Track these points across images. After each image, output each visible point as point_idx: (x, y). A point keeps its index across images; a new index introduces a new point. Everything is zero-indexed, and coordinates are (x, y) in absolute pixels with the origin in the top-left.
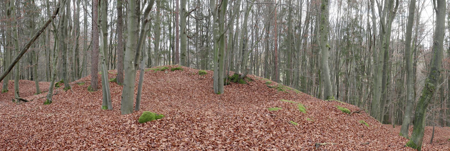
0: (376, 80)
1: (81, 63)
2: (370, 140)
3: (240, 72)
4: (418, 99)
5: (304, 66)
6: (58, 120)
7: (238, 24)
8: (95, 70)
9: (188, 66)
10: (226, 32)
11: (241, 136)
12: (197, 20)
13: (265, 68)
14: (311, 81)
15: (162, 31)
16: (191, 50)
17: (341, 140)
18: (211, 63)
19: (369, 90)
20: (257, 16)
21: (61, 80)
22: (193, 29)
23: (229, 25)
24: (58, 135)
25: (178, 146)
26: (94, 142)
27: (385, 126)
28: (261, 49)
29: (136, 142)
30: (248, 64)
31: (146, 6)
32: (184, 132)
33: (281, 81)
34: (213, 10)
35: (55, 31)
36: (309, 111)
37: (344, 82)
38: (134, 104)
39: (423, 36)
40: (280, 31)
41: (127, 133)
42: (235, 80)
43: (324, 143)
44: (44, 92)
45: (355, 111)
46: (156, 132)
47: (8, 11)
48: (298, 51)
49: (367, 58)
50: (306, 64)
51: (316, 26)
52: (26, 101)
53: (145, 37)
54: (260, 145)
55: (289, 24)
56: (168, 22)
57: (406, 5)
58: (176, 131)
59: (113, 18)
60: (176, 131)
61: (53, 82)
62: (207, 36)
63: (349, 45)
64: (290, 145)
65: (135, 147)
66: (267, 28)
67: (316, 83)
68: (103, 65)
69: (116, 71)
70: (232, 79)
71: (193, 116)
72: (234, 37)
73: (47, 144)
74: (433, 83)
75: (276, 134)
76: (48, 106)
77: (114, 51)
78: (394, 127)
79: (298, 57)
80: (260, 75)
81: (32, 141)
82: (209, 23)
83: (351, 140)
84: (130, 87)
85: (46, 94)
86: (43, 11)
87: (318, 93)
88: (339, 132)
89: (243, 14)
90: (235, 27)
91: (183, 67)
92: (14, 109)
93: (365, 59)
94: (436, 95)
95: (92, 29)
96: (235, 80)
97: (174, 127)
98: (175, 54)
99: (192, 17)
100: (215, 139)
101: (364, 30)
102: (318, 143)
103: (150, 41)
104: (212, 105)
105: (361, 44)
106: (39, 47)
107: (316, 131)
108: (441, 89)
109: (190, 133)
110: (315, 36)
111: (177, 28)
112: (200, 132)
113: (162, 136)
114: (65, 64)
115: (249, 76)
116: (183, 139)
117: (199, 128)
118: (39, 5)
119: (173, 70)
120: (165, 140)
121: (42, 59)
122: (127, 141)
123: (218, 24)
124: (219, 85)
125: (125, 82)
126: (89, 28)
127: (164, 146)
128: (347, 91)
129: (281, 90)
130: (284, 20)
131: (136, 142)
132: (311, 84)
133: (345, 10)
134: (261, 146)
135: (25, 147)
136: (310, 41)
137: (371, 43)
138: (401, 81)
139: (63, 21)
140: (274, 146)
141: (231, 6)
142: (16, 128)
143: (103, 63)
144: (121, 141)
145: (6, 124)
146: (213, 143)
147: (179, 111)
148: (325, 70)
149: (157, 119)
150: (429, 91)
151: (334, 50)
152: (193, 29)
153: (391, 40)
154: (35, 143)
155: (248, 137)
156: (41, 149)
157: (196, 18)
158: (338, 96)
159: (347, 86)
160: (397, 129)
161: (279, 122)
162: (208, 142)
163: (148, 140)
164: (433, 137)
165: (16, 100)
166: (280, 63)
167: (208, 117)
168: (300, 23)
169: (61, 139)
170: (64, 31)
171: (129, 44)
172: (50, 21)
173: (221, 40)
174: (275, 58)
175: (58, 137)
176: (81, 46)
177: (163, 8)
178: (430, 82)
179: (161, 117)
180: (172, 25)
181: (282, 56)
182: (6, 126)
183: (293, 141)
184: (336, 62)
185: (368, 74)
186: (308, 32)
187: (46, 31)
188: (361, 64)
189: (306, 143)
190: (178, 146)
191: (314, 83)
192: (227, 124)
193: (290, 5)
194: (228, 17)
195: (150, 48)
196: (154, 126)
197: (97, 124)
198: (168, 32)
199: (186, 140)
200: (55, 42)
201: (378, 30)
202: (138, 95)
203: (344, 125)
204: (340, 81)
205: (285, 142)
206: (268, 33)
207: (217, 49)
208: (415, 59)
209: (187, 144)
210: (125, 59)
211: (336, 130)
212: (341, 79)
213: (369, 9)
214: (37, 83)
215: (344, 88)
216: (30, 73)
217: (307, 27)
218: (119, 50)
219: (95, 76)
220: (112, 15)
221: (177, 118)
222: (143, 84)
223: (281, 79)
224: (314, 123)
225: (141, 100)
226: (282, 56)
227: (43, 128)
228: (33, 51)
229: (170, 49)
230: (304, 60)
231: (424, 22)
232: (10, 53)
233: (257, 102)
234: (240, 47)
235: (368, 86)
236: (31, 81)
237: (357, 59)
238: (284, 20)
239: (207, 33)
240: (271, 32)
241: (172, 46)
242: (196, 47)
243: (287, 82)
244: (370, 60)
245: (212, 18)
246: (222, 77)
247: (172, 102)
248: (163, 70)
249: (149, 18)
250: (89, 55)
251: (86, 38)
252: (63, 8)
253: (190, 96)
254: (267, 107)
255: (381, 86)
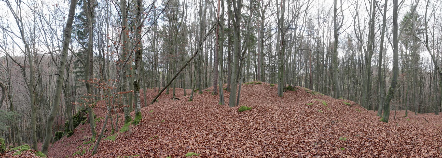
0: (364, 87)
1: (208, 80)
2: (361, 119)
3: (292, 85)
4: (386, 97)
5: (326, 81)
6: (196, 109)
7: (290, 59)
8: (216, 83)
9: (265, 82)
10: (284, 64)
11: (293, 118)
12: (269, 58)
13: (305, 82)
14: (330, 89)
15: (251, 63)
16: (266, 73)
17: (346, 119)
18: (276, 80)
19: (361, 93)
20: (300, 55)
21: (197, 88)
22: (267, 62)
23: (286, 60)
24: (196, 117)
25: (259, 123)
26: (215, 121)
27: (369, 111)
28: (303, 72)
29: (237, 121)
30: (296, 80)
31: (243, 51)
32: (262, 116)
33: (314, 89)
34: (278, 53)
35: (195, 63)
36: (328, 105)
37: (347, 89)
38: (236, 102)
39: (388, 63)
40: (313, 63)
41: (232, 117)
42: (289, 89)
43: (337, 121)
44: (189, 95)
45: (353, 104)
46: (248, 117)
47: (171, 52)
48: (322, 73)
49: (359, 76)
50: (327, 80)
51: (332, 60)
52: (179, 99)
53: (242, 67)
54: (302, 122)
55: (318, 59)
56: (254, 58)
57: (379, 47)
58: (258, 116)
59: (226, 56)
60: (258, 116)
61: (194, 89)
62: (274, 66)
63: (349, 69)
64: (318, 123)
65: (237, 124)
66: (306, 61)
67: (332, 90)
68: (220, 81)
69: (227, 84)
70: (288, 89)
71: (267, 108)
72: (288, 66)
73: (190, 122)
74: (393, 88)
75: (311, 117)
76: (191, 102)
77: (225, 73)
78: (375, 112)
79: (323, 76)
80: (302, 86)
81: (182, 120)
82: (276, 59)
83: (351, 119)
84: (234, 93)
85: (189, 96)
86: (189, 52)
87: (333, 95)
88: (344, 115)
89: (293, 54)
90: (289, 61)
91: (262, 82)
92: (173, 103)
93: (358, 77)
94: (397, 93)
95: (214, 62)
96: (289, 89)
97: (257, 114)
98: (258, 75)
99: (267, 56)
100: (279, 120)
101: (357, 61)
102: (333, 121)
103: (244, 69)
104: (277, 102)
105: (356, 69)
106: (186, 71)
107: (332, 115)
108: (399, 91)
109: (266, 117)
110: (331, 65)
111: (259, 62)
112: (271, 117)
113: (251, 118)
114: (200, 80)
115: (296, 87)
116: (261, 120)
117: (270, 114)
118: (187, 49)
119: (256, 84)
120: (252, 120)
121: (188, 77)
122: (232, 121)
123: (280, 60)
124: (281, 92)
125: (231, 90)
126: (212, 61)
127: (252, 123)
128: (349, 94)
129: (314, 94)
130: (315, 57)
131: (237, 121)
132: (330, 90)
133: (347, 51)
134: (303, 123)
135: (178, 123)
136: (329, 68)
137: (361, 68)
138: (378, 87)
139: (199, 58)
140: (310, 123)
141: (287, 50)
142: (173, 113)
143: (220, 80)
144: (229, 121)
145: (168, 111)
146: (278, 122)
147: (260, 106)
148: (337, 83)
149: (248, 110)
150: (392, 92)
151: (341, 72)
152: (267, 62)
153: (371, 66)
154: (184, 121)
155: (296, 119)
156: (187, 124)
157: (269, 57)
158: (344, 96)
159: (349, 91)
160: (376, 113)
161: (313, 111)
162: (275, 121)
163: (244, 120)
164: (395, 116)
165: (174, 99)
166: (313, 80)
167: (275, 109)
168: (323, 58)
169: (197, 120)
170: (200, 63)
171: (233, 70)
172: (193, 58)
173: (282, 68)
174: (310, 77)
175: (196, 118)
176: (208, 71)
177: (251, 52)
178: (392, 87)
179: (250, 109)
180: (256, 60)
181: (314, 76)
182: (168, 112)
183: (320, 120)
184: (343, 78)
185: (360, 84)
186: (327, 63)
187: (190, 63)
188: (356, 79)
189: (327, 121)
190: (259, 123)
191: (331, 90)
192: (285, 112)
193: (318, 50)
194: (285, 56)
195: (244, 72)
196: (247, 113)
197: (216, 112)
198: (254, 64)
199: (264, 120)
200: (195, 69)
201: (364, 61)
202: (238, 97)
203: (347, 111)
204: (345, 88)
205: (316, 121)
206: (306, 64)
207: (280, 73)
208: (385, 75)
209: (264, 123)
210: (231, 78)
211: (343, 114)
212: (346, 87)
213: (359, 50)
214: (185, 90)
215: (347, 92)
216: (181, 84)
217: (327, 60)
218: (228, 73)
219: (216, 87)
220: (225, 55)
221: (259, 109)
222: (241, 91)
223: (314, 88)
224: (331, 111)
225: (240, 100)
226: (314, 76)
227: (188, 114)
228: (183, 73)
229: (255, 73)
230: (326, 78)
231: (388, 56)
232: (171, 74)
233: (301, 100)
234: (292, 71)
235: (360, 91)
236: (181, 89)
237: (354, 77)
238: (315, 57)
239: (275, 64)
240: (308, 63)
241: (256, 71)
242: (269, 71)
243: (317, 90)
244: (360, 77)
245: (277, 57)
246: (283, 88)
247: (256, 101)
248: (251, 84)
249: (244, 57)
250: (213, 75)
251: (211, 67)
252: (200, 52)
253: (266, 98)
254: (306, 103)
255: (367, 90)
